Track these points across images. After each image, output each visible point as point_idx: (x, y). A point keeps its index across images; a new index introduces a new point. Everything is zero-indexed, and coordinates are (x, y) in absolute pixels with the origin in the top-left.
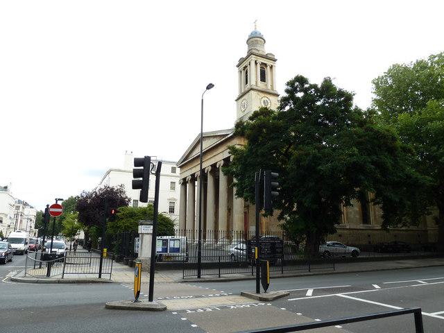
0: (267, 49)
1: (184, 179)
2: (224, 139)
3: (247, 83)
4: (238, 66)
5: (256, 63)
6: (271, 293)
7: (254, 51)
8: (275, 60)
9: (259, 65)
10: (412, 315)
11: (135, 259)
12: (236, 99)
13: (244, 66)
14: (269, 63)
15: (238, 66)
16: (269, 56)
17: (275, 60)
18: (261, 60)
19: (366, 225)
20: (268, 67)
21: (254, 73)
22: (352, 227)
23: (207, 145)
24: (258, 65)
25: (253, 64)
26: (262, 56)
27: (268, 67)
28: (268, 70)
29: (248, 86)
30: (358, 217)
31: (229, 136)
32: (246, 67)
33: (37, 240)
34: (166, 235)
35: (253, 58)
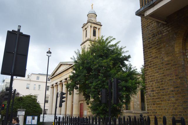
0: (98, 20)
1: (52, 85)
2: (71, 66)
6: (140, 114)
7: (90, 21)
8: (101, 26)
9: (92, 28)
10: (33, 120)
11: (26, 110)
13: (85, 28)
14: (98, 27)
15: (82, 28)
16: (97, 23)
17: (101, 26)
18: (93, 25)
19: (143, 111)
20: (97, 29)
21: (90, 31)
22: (135, 112)
23: (62, 68)
24: (92, 28)
25: (89, 27)
26: (94, 23)
27: (97, 29)
28: (97, 30)
29: (87, 38)
30: (139, 107)
32: (86, 28)
33: (175, 111)
34: (178, 120)
35: (89, 24)
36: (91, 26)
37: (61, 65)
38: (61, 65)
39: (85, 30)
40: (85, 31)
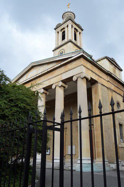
3: (63, 38)
4: (55, 29)
5: (72, 27)
9: (73, 28)
12: (53, 49)
13: (76, 28)
15: (55, 29)
18: (75, 26)
21: (70, 35)
24: (73, 28)
25: (70, 26)
28: (78, 34)
31: (73, 58)
36: (72, 25)
37: (33, 67)
38: (33, 67)
39: (60, 32)
40: (61, 34)
